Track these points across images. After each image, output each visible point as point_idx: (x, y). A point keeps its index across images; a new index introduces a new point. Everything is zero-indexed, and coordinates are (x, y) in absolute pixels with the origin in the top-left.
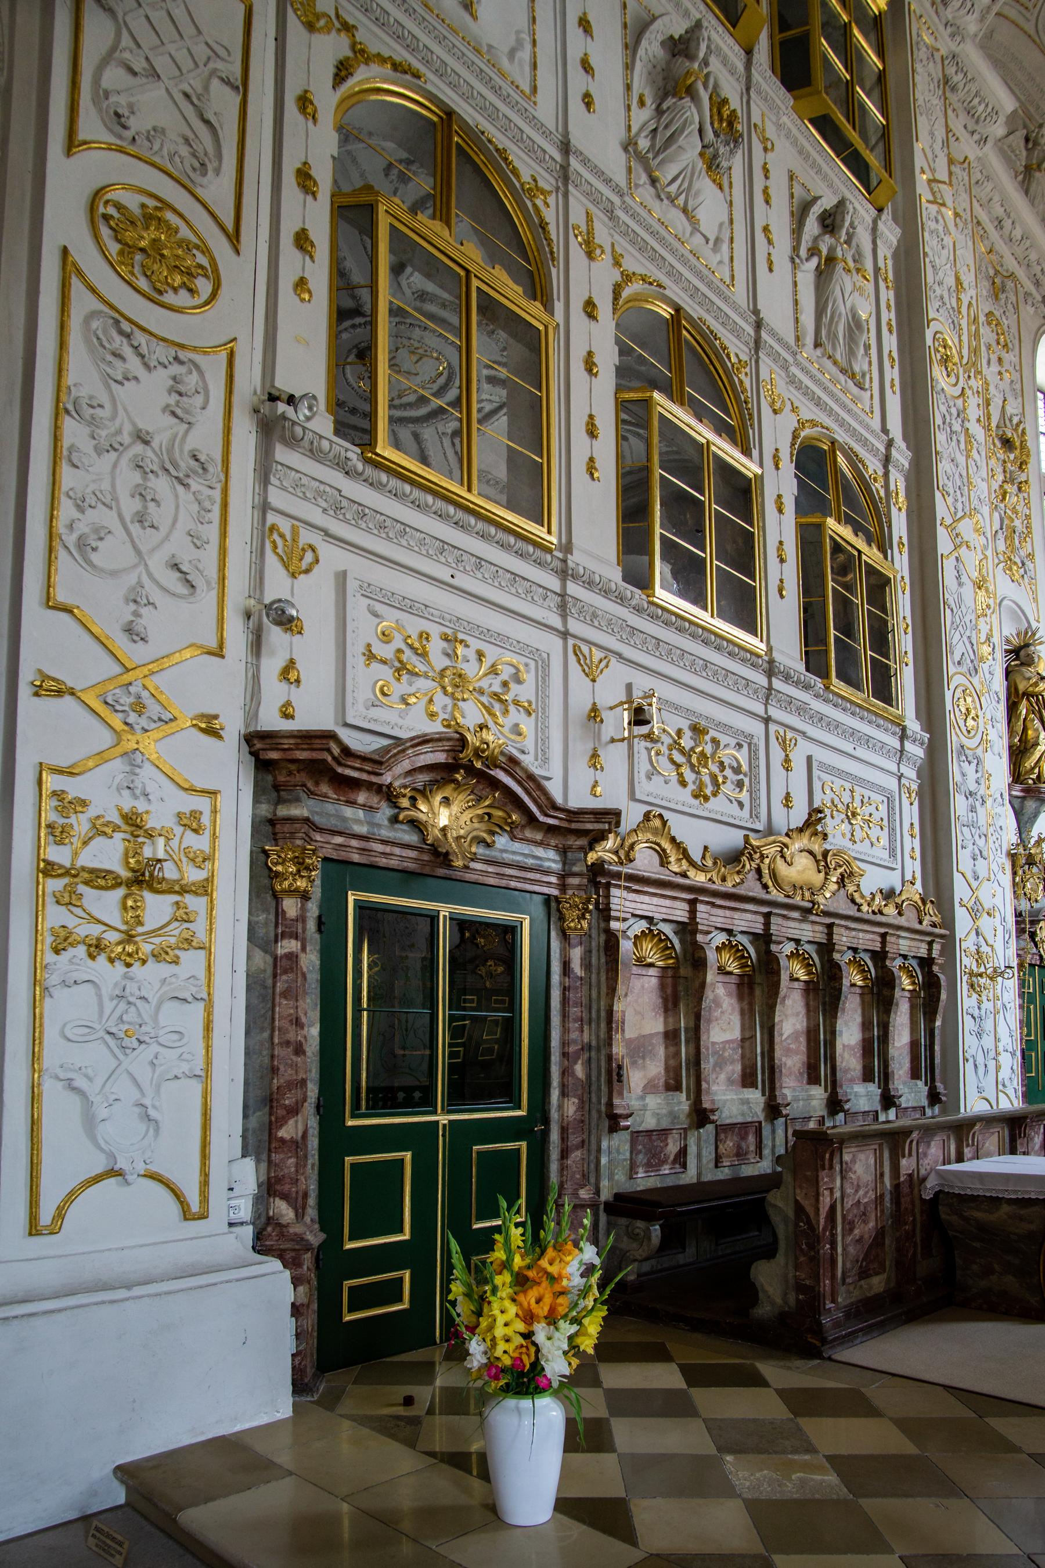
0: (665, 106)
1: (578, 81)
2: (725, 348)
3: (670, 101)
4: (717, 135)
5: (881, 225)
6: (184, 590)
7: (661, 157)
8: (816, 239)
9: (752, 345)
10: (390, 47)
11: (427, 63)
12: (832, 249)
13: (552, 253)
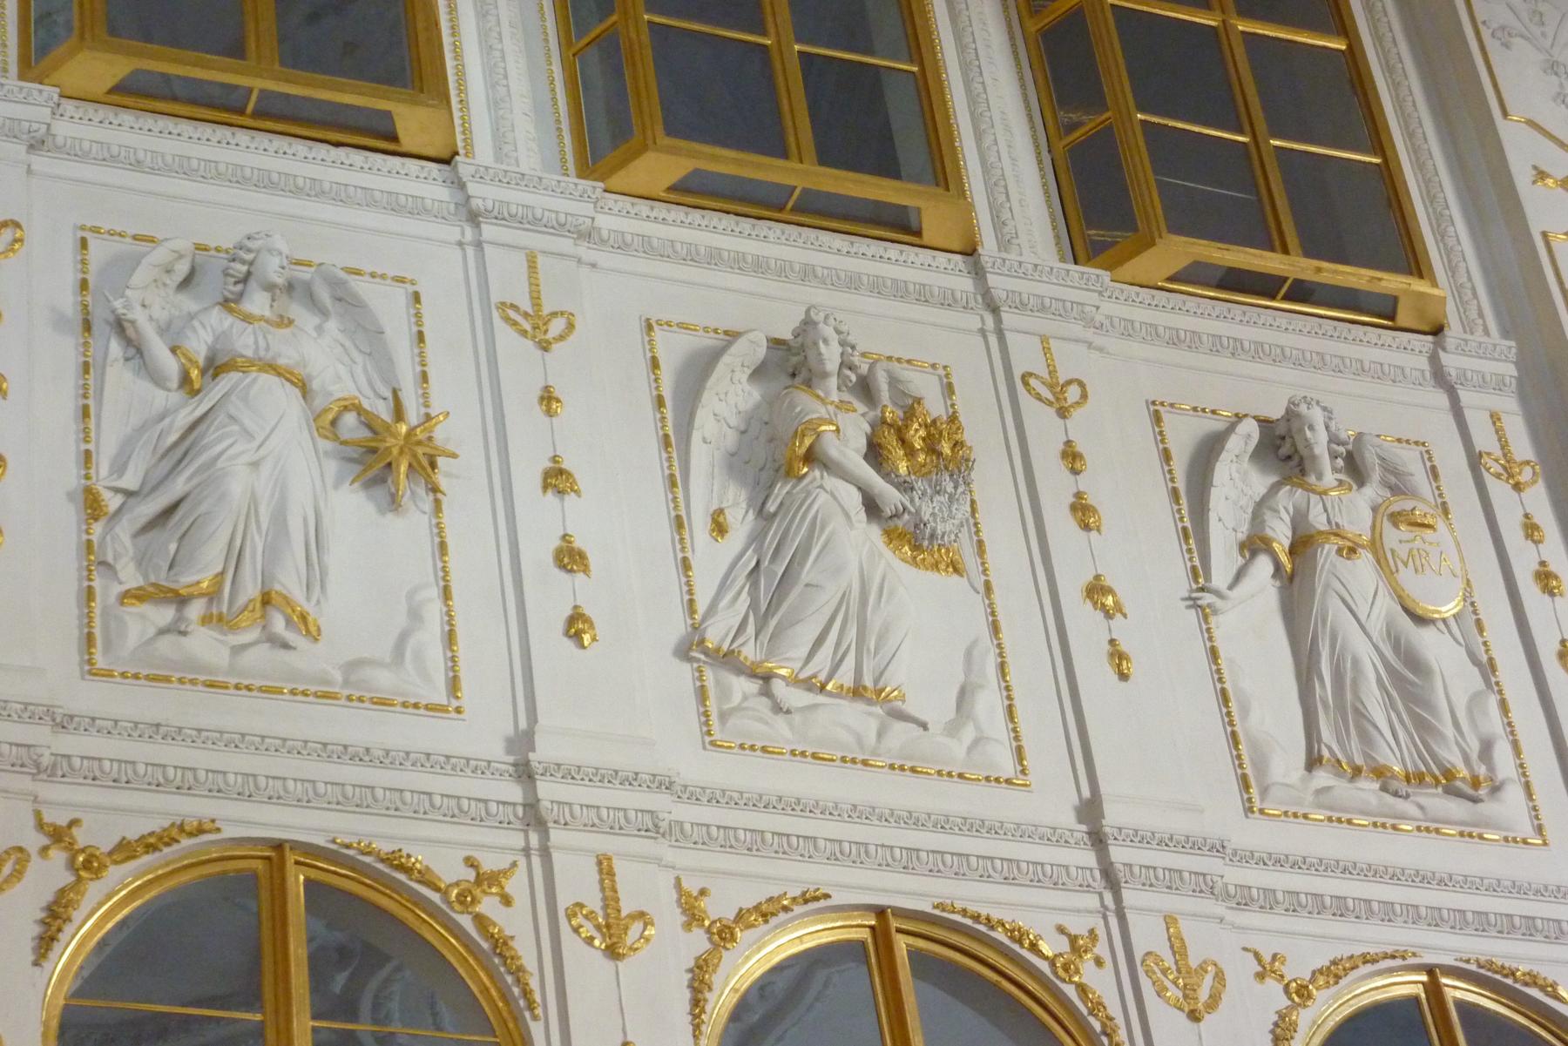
0: (771, 507)
1: (553, 597)
2: (1018, 935)
3: (781, 490)
4: (905, 487)
5: (1449, 361)
6: (161, 451)
7: (773, 623)
8: (1261, 506)
9: (1099, 882)
10: (142, 812)
11: (219, 792)
12: (1299, 520)
13: (526, 993)
